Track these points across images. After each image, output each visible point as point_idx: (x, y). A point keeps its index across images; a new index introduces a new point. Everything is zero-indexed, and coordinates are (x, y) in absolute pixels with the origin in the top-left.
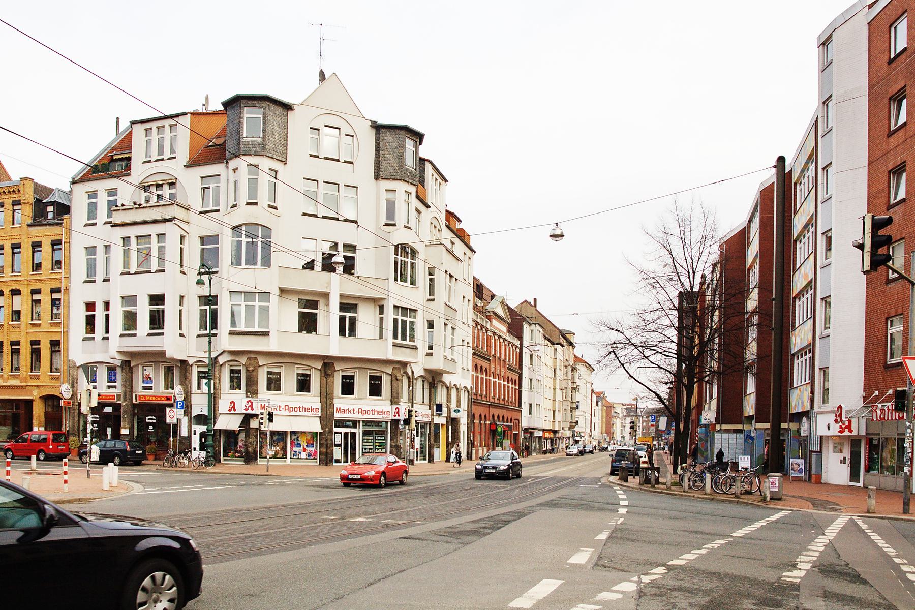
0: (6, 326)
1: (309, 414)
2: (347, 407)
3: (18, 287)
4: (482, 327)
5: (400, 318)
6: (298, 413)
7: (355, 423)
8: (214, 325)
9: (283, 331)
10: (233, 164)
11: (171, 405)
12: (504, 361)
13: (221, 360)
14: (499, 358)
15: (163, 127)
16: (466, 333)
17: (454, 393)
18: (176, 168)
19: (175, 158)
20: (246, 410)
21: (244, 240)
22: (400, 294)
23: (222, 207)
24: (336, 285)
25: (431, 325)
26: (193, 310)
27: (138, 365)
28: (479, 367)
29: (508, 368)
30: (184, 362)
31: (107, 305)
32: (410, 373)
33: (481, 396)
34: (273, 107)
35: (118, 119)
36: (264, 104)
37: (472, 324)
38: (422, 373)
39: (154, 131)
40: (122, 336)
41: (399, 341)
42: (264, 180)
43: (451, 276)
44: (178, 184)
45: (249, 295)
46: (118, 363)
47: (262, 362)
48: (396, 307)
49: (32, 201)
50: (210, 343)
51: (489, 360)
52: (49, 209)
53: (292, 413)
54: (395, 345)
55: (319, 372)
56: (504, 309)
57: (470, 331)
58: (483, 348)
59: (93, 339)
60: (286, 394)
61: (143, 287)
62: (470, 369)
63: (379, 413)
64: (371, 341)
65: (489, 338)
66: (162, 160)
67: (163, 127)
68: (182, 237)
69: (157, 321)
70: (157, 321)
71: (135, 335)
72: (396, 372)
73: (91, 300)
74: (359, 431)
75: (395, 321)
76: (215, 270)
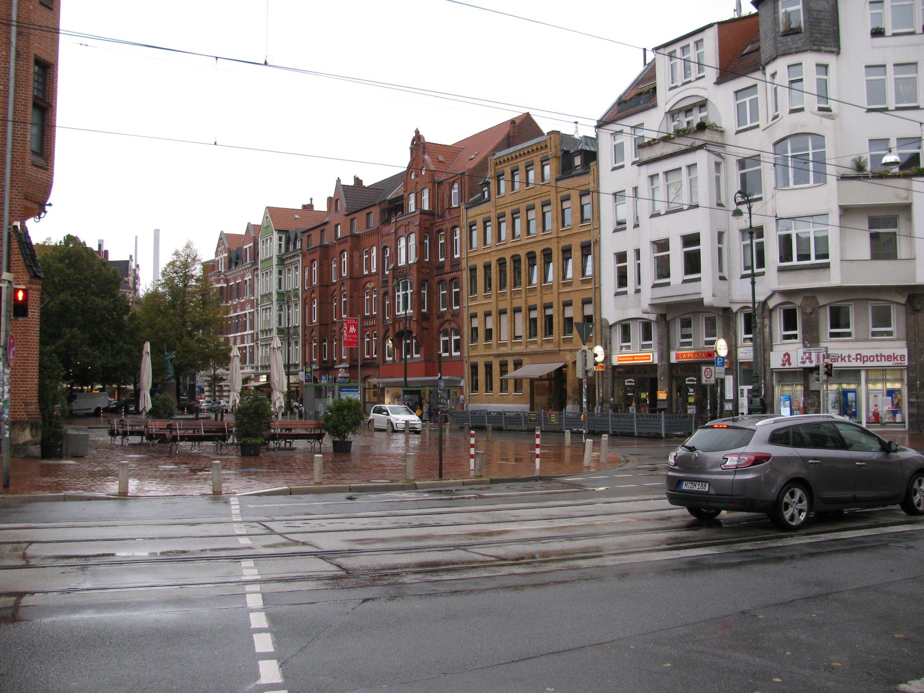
0: (539, 288)
3: (518, 253)
8: (761, 264)
10: (770, 70)
11: (712, 363)
13: (771, 304)
15: (688, 45)
19: (703, 77)
20: (803, 362)
23: (762, 122)
26: (736, 246)
27: (675, 318)
30: (727, 310)
31: (638, 252)
35: (157, 233)
39: (679, 54)
40: (655, 286)
44: (709, 106)
46: (653, 317)
47: (822, 301)
50: (753, 283)
52: (575, 158)
55: (903, 309)
60: (857, 340)
61: (674, 229)
63: (888, 358)
66: (690, 82)
67: (688, 45)
68: (717, 165)
69: (693, 263)
70: (693, 263)
71: (668, 284)
73: (622, 250)
76: (755, 197)
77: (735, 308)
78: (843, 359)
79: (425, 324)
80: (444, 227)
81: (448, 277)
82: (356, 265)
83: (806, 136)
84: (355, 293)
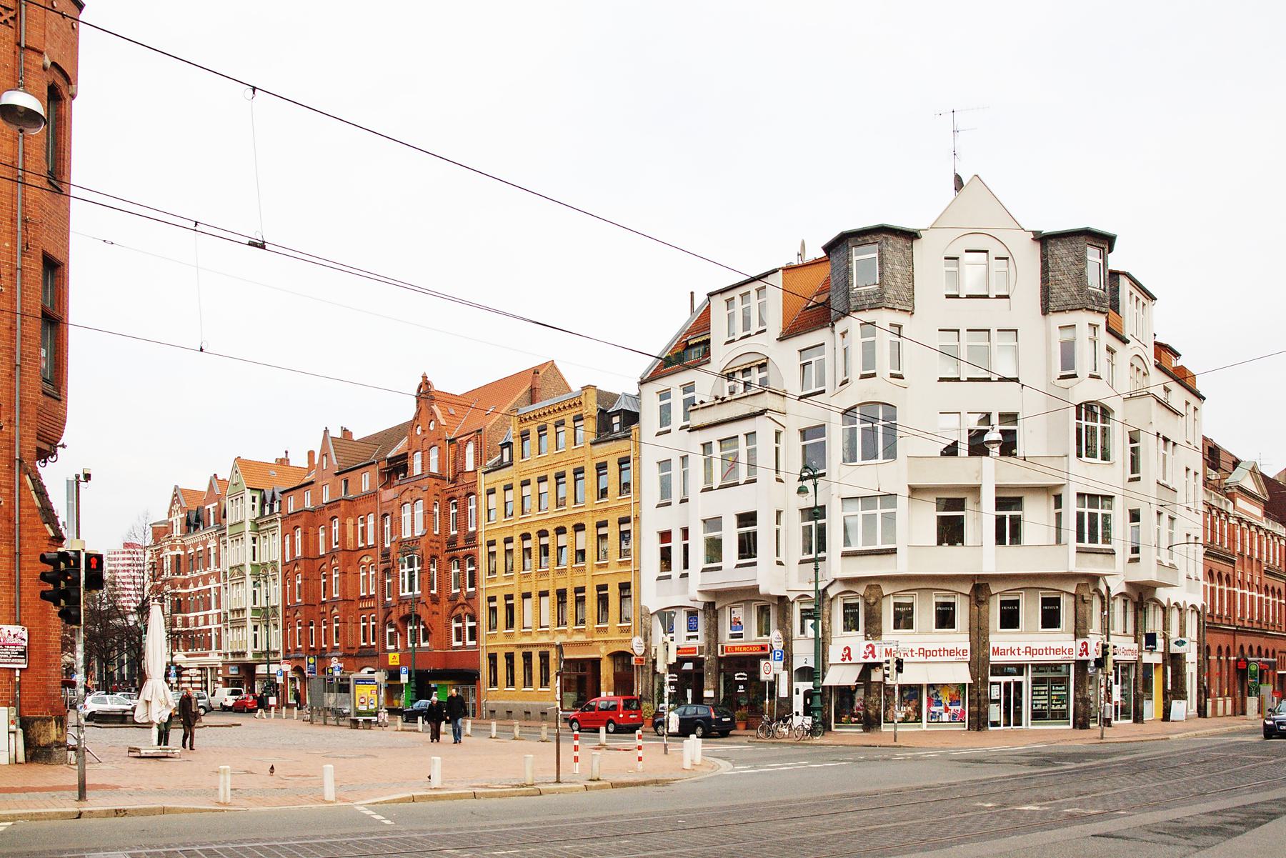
1: (952, 659)
2: (1007, 645)
4: (1220, 511)
5: (1087, 511)
6: (938, 659)
7: (1020, 669)
9: (916, 546)
12: (1259, 561)
13: (832, 592)
14: (1250, 558)
16: (1192, 523)
17: (1174, 616)
18: (766, 345)
21: (859, 426)
22: (1087, 475)
24: (991, 473)
25: (1135, 516)
28: (1224, 575)
29: (1266, 572)
32: (1104, 591)
33: (1220, 617)
34: (892, 239)
36: (879, 238)
37: (1202, 508)
38: (1123, 589)
41: (1086, 544)
42: (884, 340)
43: (1166, 440)
45: (867, 500)
48: (1080, 495)
49: (595, 413)
51: (1233, 562)
53: (930, 659)
54: (1079, 551)
56: (1256, 481)
57: (1200, 519)
58: (1221, 543)
59: (669, 577)
62: (1201, 576)
64: (1044, 548)
65: (1231, 529)
72: (1080, 591)
74: (1026, 679)
75: (1080, 516)
77: (792, 597)
78: (1013, 652)
79: (435, 608)
80: (457, 494)
81: (461, 553)
82: (350, 535)
83: (875, 406)
84: (349, 569)
